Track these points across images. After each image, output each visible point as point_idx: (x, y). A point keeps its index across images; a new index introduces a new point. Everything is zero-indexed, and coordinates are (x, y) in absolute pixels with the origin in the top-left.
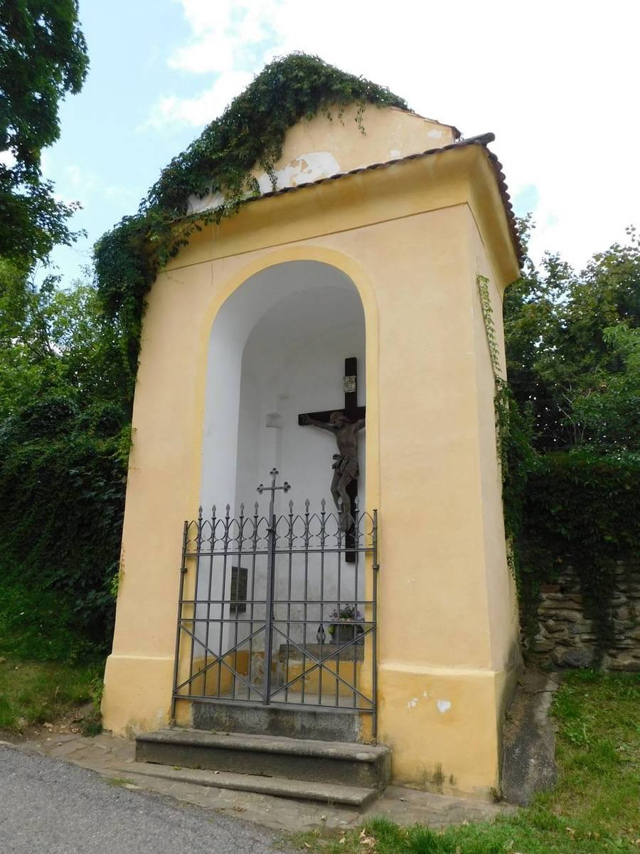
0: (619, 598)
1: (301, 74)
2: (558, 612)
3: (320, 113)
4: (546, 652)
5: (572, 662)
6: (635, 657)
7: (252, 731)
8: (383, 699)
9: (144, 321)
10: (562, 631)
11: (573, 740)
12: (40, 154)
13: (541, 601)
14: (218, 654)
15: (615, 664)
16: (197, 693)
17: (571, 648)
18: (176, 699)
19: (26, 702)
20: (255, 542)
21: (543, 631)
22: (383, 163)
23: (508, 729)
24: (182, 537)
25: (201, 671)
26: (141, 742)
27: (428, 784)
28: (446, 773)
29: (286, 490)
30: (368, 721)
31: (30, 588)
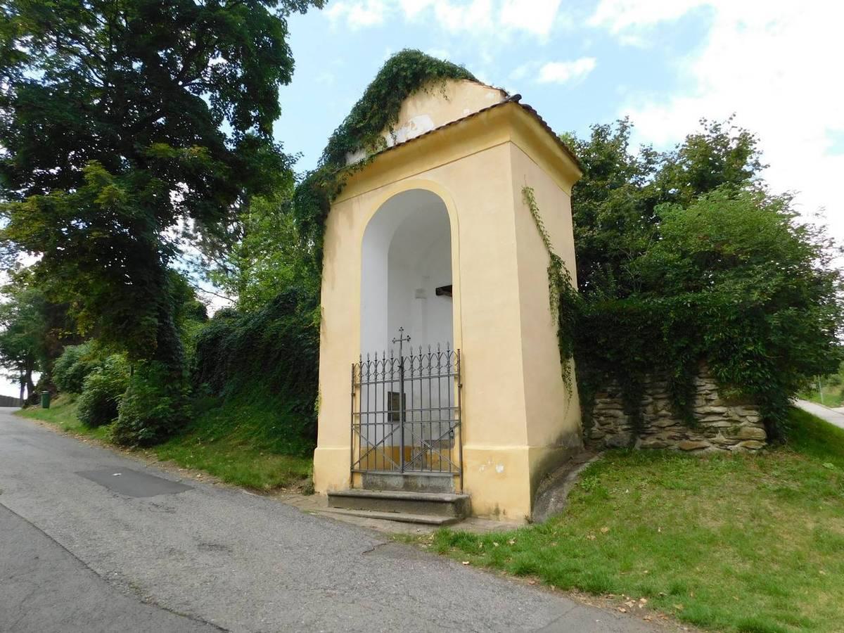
0: (647, 399)
1: (406, 65)
2: (607, 411)
3: (421, 89)
4: (600, 439)
5: (615, 444)
6: (658, 439)
7: (394, 489)
8: (466, 466)
9: (325, 238)
10: (609, 424)
11: (584, 487)
12: (272, 125)
13: (596, 404)
14: (374, 444)
15: (645, 444)
16: (364, 469)
17: (615, 435)
18: (353, 473)
19: (271, 476)
20: (392, 374)
21: (597, 424)
22: (455, 120)
23: (694, 515)
24: (351, 374)
25: (366, 455)
26: (330, 496)
27: (491, 516)
28: (501, 509)
29: (408, 340)
30: (458, 480)
31: (279, 413)
